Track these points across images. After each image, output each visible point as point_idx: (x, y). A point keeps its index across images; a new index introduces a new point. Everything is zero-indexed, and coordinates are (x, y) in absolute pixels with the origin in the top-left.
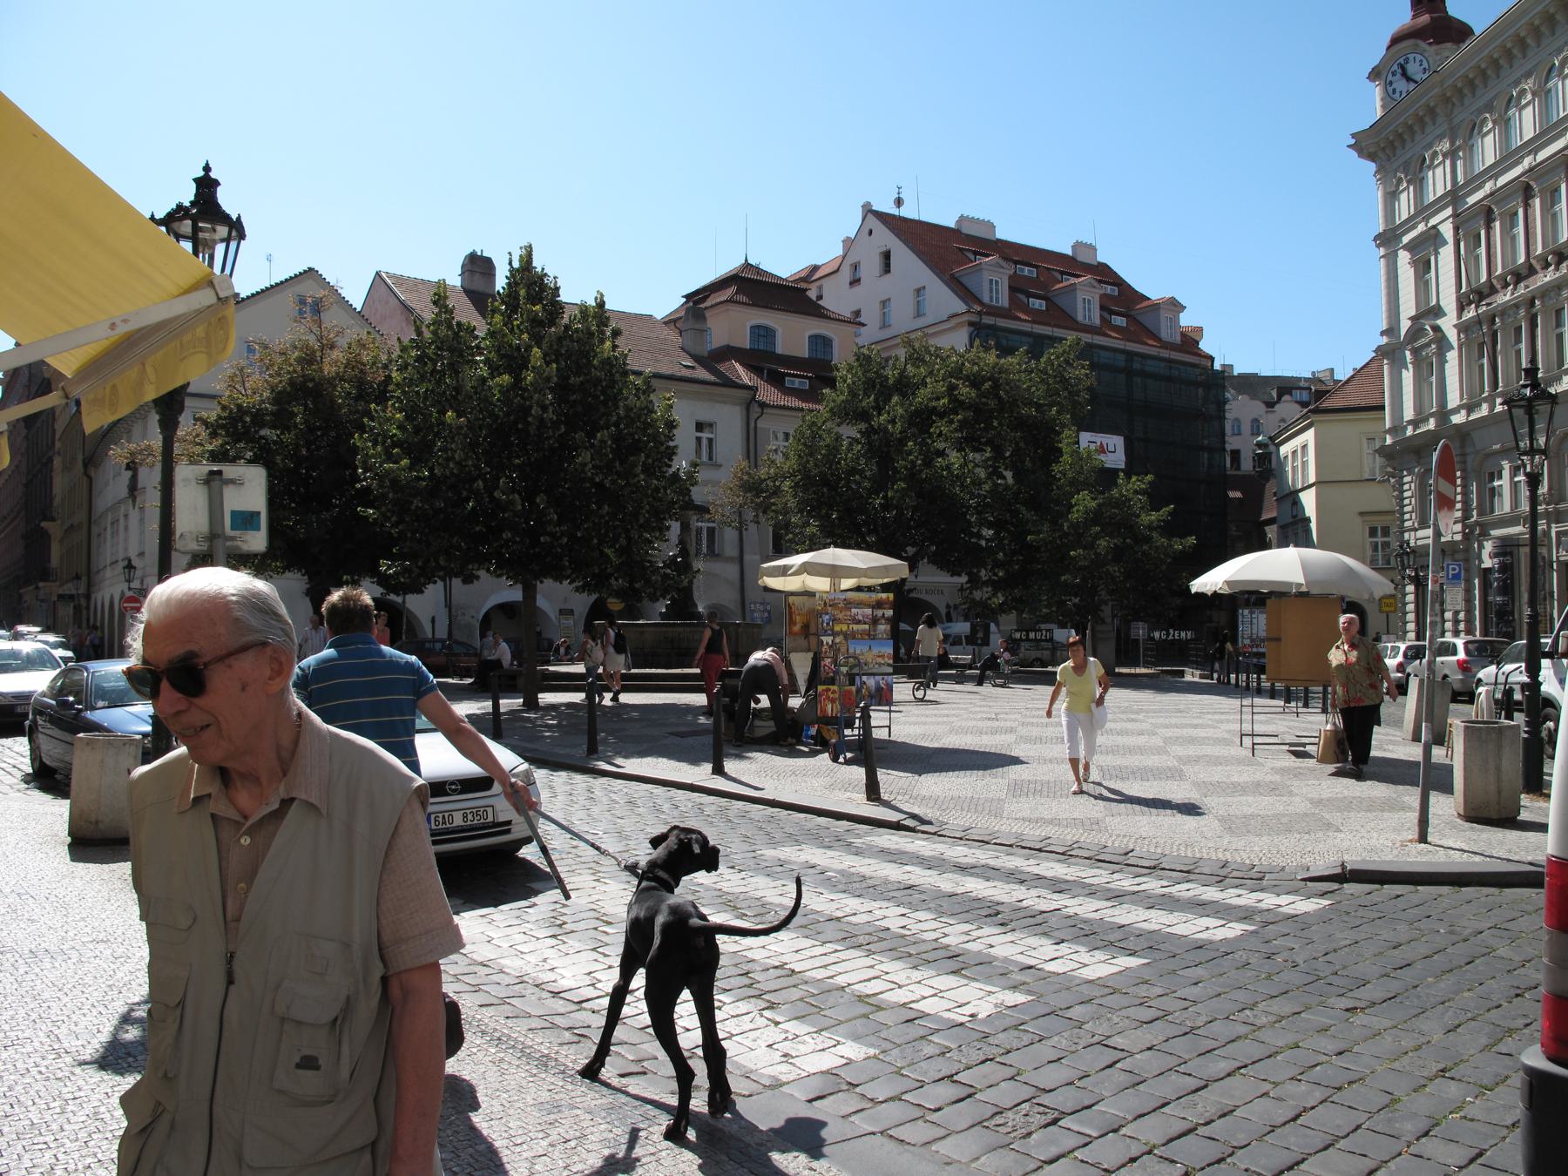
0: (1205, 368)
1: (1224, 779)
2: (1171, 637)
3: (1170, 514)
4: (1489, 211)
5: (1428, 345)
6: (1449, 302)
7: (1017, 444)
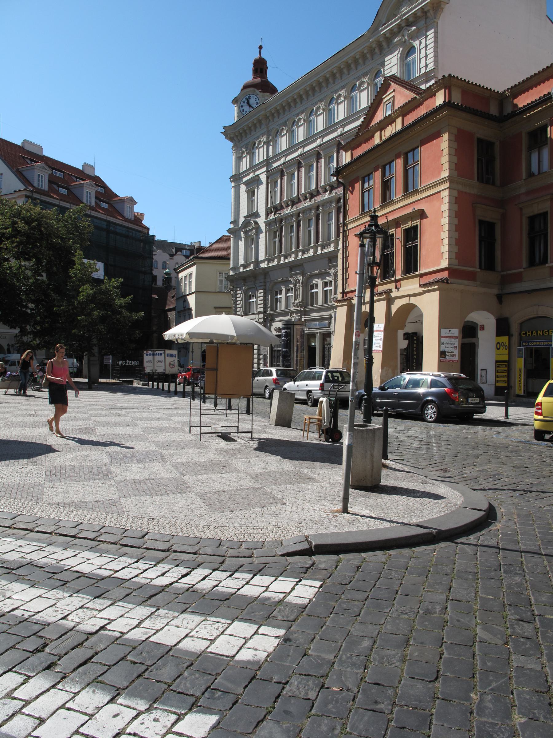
0: (145, 233)
1: (190, 460)
2: (127, 364)
3: (131, 300)
4: (282, 171)
5: (251, 230)
6: (262, 211)
7: (50, 257)
